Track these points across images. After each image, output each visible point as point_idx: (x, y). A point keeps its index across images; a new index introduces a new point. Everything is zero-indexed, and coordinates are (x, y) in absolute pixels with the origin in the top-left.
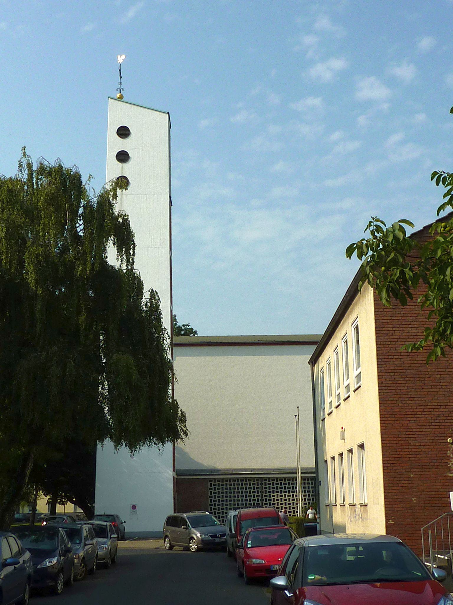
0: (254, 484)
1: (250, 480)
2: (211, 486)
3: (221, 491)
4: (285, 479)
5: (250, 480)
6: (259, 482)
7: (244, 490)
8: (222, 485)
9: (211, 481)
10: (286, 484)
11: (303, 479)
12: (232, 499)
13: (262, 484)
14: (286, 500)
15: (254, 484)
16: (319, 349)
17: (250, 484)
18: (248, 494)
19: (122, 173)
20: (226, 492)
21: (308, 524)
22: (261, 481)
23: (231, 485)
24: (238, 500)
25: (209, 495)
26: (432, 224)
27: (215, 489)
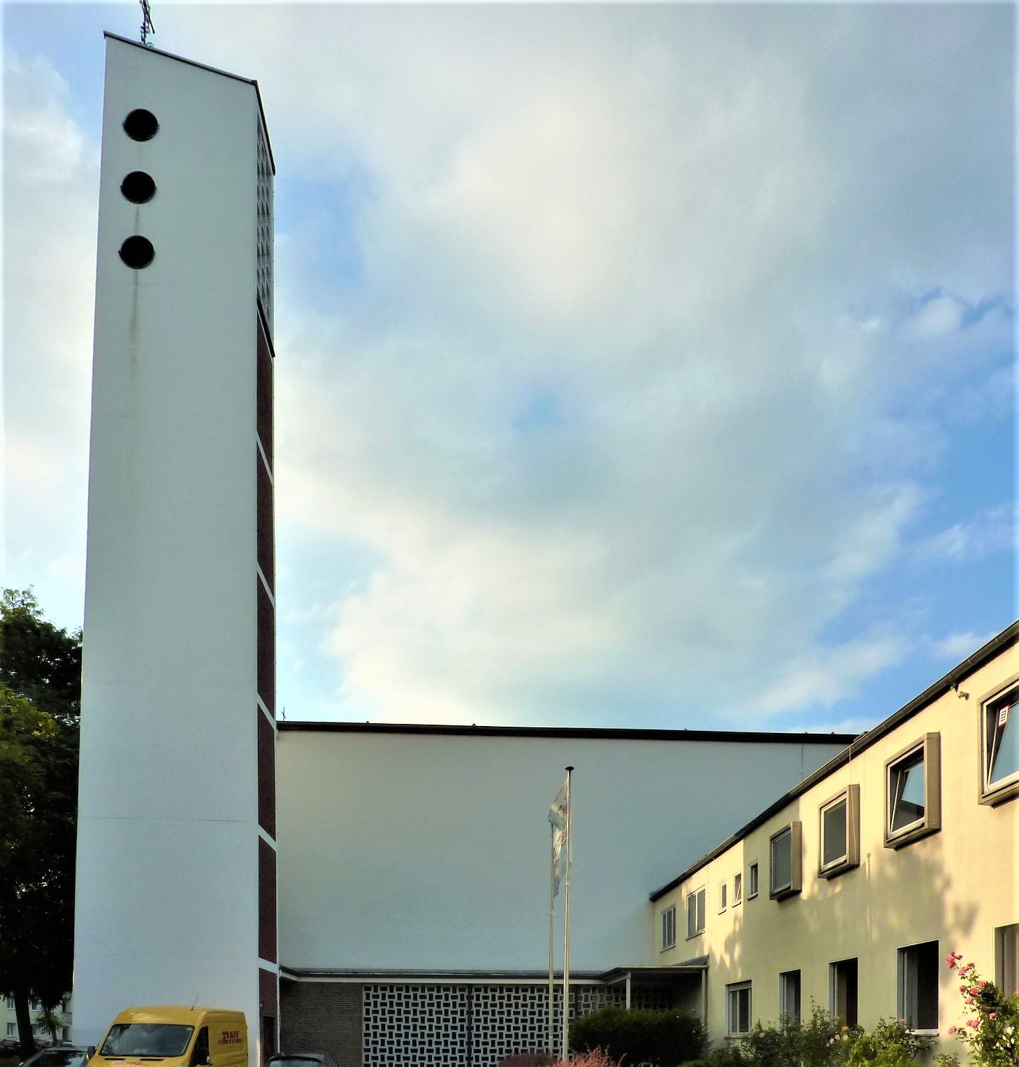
0: (486, 998)
1: (494, 990)
2: (368, 997)
3: (505, 1017)
4: (517, 987)
5: (431, 989)
6: (466, 994)
7: (513, 1009)
8: (438, 997)
9: (369, 989)
10: (377, 997)
11: (574, 988)
12: (505, 1040)
13: (470, 998)
14: (501, 1013)
15: (486, 998)
16: (879, 733)
17: (447, 996)
18: (505, 1017)
19: (138, 207)
20: (501, 1022)
21: (278, 1007)
22: (470, 992)
23: (424, 997)
24: (421, 1028)
25: (364, 1031)
26: (855, 736)
27: (431, 1012)
